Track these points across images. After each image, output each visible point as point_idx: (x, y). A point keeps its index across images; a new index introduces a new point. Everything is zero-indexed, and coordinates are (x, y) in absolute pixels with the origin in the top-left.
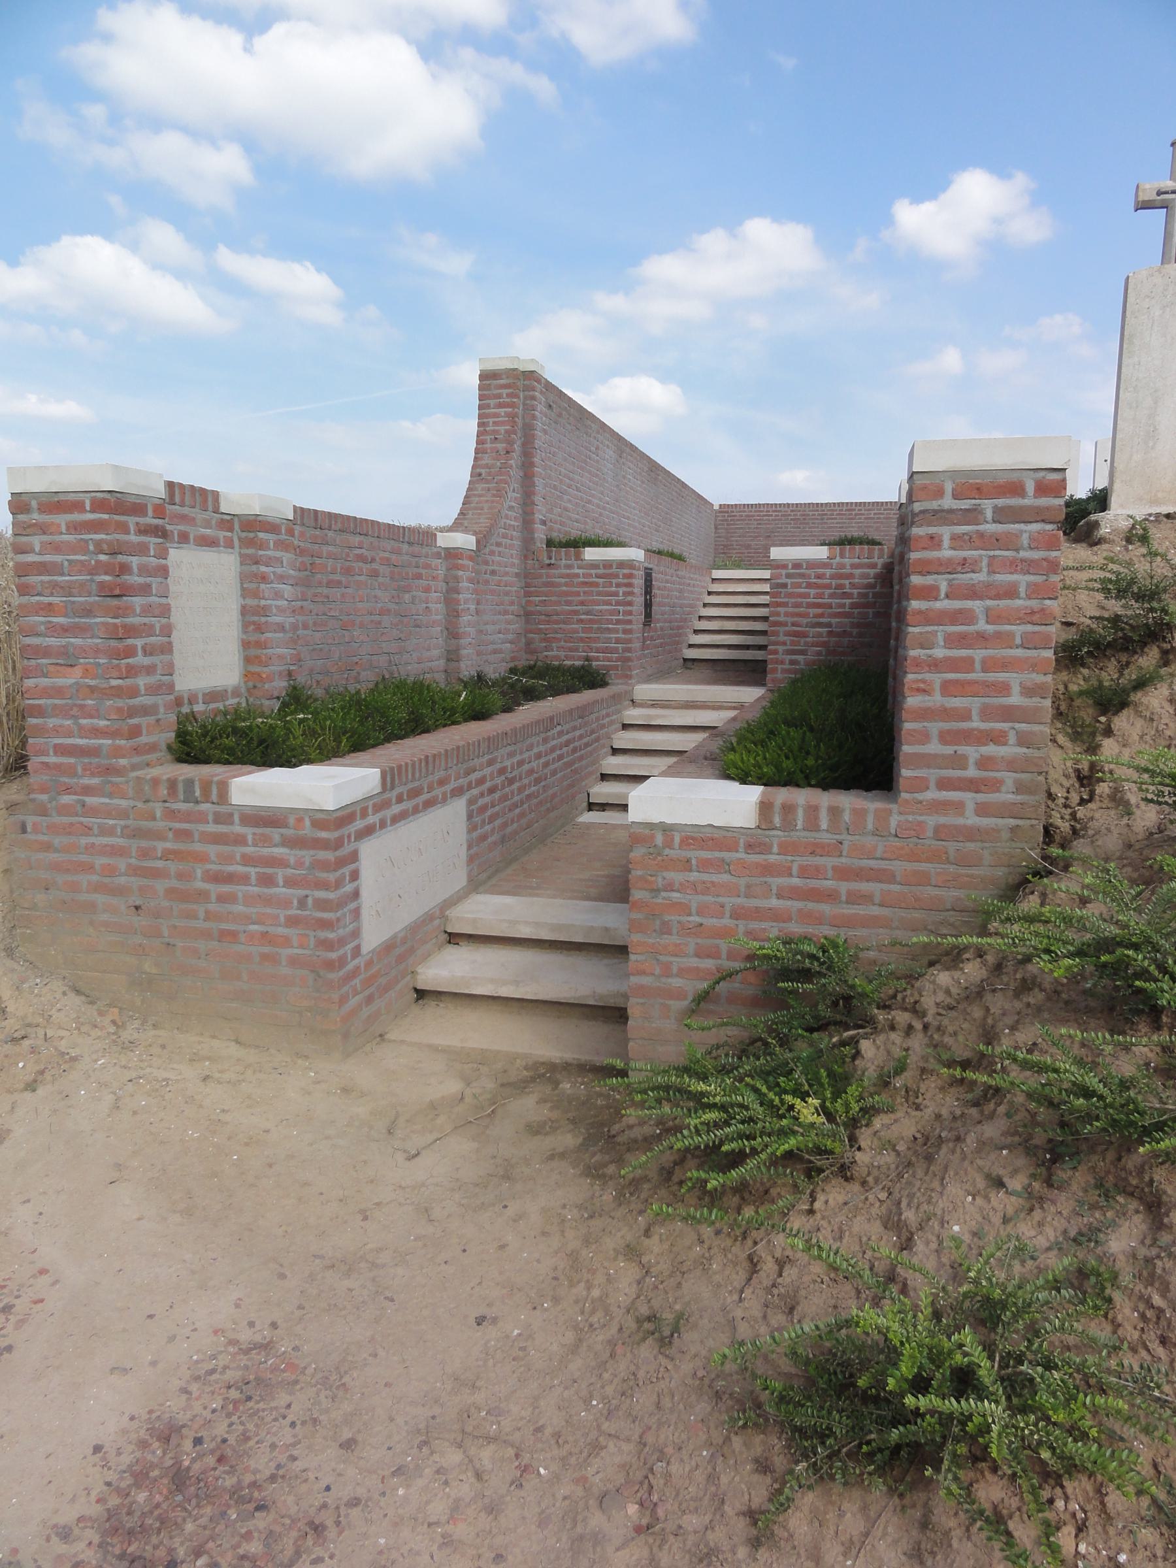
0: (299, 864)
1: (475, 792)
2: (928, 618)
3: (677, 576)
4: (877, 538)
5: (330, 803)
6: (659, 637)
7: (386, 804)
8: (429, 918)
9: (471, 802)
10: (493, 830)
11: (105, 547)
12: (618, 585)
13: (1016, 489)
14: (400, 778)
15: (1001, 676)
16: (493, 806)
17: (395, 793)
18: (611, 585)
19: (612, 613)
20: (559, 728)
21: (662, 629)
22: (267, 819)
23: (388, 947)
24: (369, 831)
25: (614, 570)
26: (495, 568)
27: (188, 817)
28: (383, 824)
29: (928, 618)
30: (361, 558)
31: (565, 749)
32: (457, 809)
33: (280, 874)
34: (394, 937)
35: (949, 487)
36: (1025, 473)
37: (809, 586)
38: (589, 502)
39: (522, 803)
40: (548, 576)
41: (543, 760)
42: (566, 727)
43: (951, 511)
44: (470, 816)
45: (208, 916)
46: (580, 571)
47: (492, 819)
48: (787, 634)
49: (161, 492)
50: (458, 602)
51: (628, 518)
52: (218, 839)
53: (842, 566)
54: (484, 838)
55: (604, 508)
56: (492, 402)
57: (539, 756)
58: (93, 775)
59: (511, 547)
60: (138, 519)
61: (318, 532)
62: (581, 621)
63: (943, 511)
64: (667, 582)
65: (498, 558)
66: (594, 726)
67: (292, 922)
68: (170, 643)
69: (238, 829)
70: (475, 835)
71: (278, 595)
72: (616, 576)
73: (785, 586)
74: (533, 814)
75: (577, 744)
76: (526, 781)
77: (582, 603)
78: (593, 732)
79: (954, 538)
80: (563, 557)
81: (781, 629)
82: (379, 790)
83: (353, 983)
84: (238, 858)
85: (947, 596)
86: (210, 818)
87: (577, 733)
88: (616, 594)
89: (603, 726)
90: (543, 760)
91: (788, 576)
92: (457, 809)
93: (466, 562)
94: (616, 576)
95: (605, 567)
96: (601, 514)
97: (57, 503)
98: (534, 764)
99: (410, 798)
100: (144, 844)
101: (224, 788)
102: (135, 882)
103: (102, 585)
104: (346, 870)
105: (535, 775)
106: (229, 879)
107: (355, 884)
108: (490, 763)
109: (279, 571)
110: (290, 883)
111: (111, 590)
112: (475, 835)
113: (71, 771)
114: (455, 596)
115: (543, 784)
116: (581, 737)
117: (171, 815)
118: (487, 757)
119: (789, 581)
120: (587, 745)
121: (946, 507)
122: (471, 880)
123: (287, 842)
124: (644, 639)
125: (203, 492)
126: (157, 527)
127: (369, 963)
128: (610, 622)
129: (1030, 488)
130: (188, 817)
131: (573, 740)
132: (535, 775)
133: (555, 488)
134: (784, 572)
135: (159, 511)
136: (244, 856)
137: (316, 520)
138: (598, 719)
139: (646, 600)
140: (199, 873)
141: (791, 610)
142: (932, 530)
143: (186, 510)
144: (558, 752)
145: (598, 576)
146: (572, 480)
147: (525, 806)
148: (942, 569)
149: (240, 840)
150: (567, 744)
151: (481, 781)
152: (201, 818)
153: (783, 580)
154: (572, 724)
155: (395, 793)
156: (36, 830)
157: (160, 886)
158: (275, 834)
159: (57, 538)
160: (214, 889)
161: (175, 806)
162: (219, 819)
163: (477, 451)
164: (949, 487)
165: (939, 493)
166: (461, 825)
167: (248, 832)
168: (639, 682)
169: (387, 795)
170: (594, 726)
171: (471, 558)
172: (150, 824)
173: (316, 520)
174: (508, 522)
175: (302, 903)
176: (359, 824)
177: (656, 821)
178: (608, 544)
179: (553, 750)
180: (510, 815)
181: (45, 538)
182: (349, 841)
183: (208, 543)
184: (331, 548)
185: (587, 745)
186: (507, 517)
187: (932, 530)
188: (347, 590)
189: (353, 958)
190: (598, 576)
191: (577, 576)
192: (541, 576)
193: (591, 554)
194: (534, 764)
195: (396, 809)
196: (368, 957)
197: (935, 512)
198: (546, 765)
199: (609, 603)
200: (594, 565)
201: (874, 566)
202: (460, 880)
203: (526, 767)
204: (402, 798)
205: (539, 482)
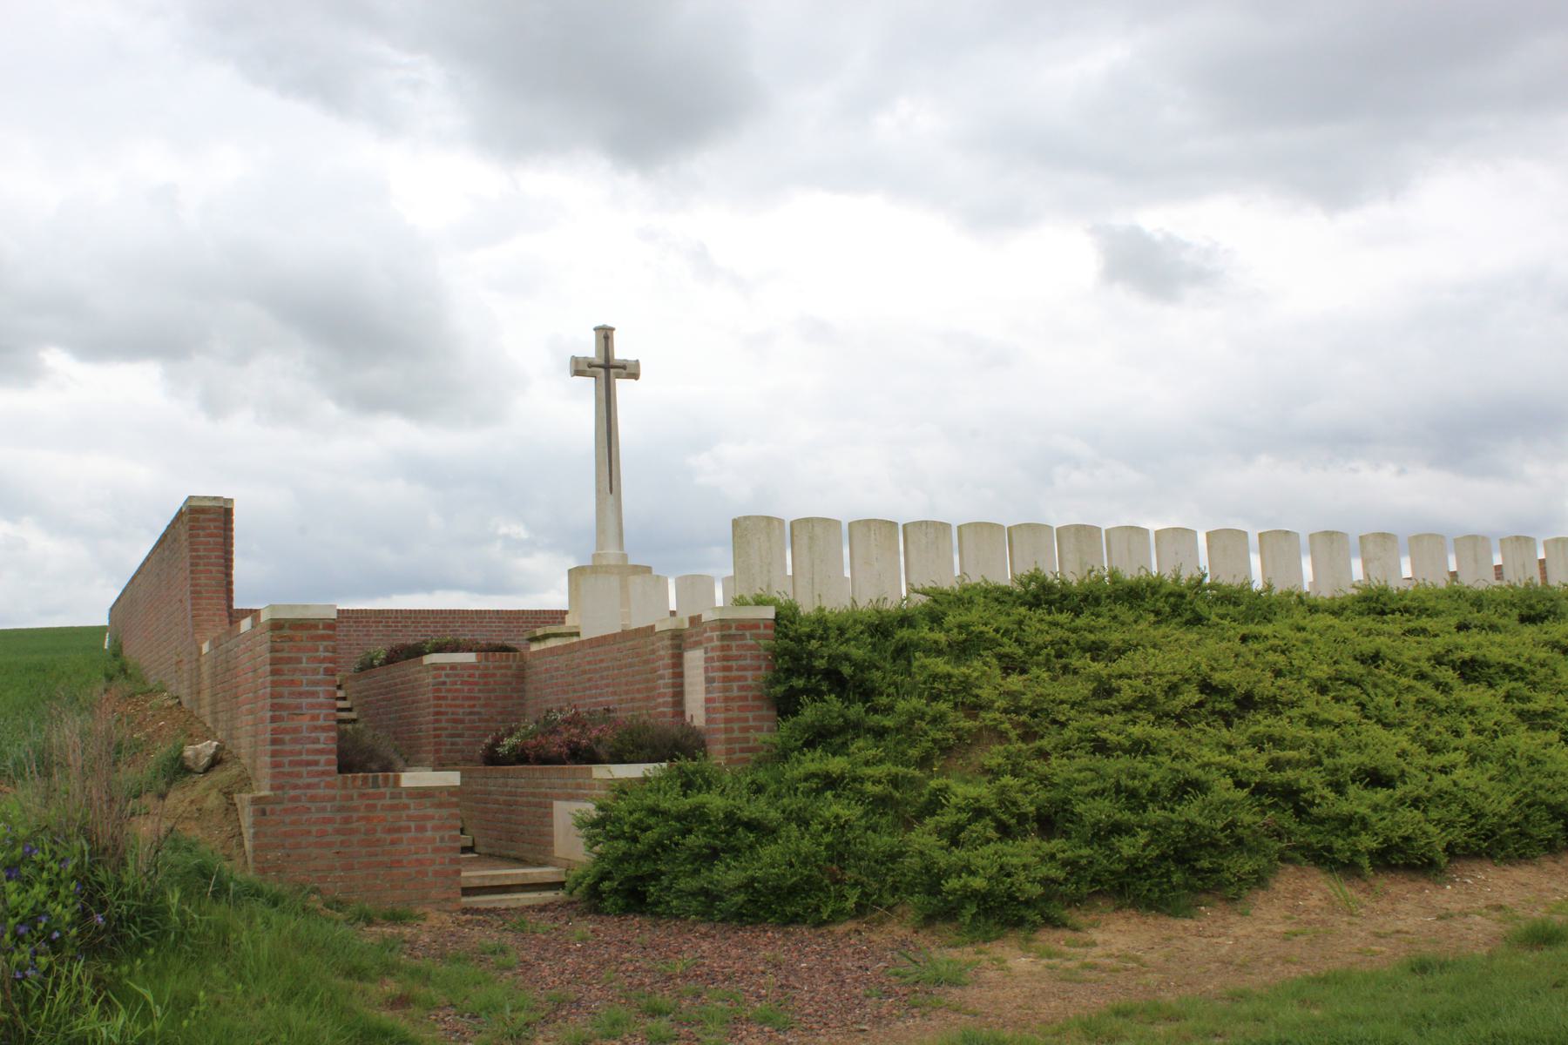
0: (441, 818)
27: (373, 796)
33: (429, 824)
37: (463, 683)
49: (334, 616)
53: (486, 668)
69: (405, 800)
91: (447, 676)
100: (345, 814)
106: (399, 830)
110: (435, 828)
113: (299, 775)
117: (362, 796)
123: (433, 805)
130: (373, 796)
140: (379, 828)
149: (406, 807)
152: (382, 796)
156: (273, 812)
158: (427, 802)
160: (389, 837)
162: (393, 797)
165: (730, 628)
167: (412, 803)
175: (442, 839)
193: (431, 659)
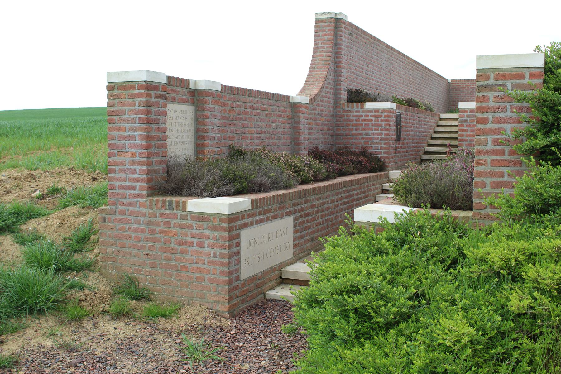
1: (298, 215)
3: (417, 116)
5: (226, 211)
6: (405, 147)
7: (253, 215)
8: (273, 269)
9: (295, 219)
10: (307, 234)
11: (142, 103)
12: (382, 121)
13: (521, 76)
14: (260, 204)
15: (386, 137)
16: (308, 222)
17: (258, 210)
18: (378, 121)
19: (378, 134)
20: (345, 189)
21: (407, 143)
22: (202, 218)
23: (253, 278)
24: (245, 226)
25: (380, 114)
26: (320, 112)
28: (252, 224)
30: (252, 108)
31: (348, 200)
32: (289, 221)
33: (206, 242)
34: (256, 275)
35: (492, 76)
36: (526, 69)
38: (373, 80)
39: (323, 223)
40: (347, 116)
41: (335, 203)
42: (348, 189)
43: (493, 86)
44: (295, 226)
46: (364, 114)
47: (307, 228)
50: (299, 128)
51: (396, 87)
52: (181, 226)
54: (302, 237)
55: (381, 83)
56: (321, 34)
57: (333, 201)
58: (132, 198)
59: (329, 102)
60: (155, 92)
61: (232, 96)
62: (363, 138)
63: (489, 85)
64: (410, 119)
65: (322, 108)
66: (365, 189)
67: (210, 263)
68: (166, 144)
69: (189, 222)
70: (298, 234)
71: (213, 124)
72: (381, 116)
73: (466, 121)
74: (329, 229)
75: (355, 197)
76: (326, 213)
77: (364, 130)
78: (364, 192)
79: (495, 97)
80: (355, 107)
81: (464, 143)
82: (250, 208)
83: (236, 292)
84: (189, 235)
85: (492, 122)
86: (179, 217)
87: (355, 192)
88: (381, 125)
89: (371, 190)
90: (335, 203)
91: (468, 116)
92: (289, 221)
93: (304, 109)
94: (381, 116)
95: (375, 112)
96: (379, 86)
97: (125, 86)
98: (330, 205)
99: (265, 213)
100: (151, 227)
101: (185, 204)
102: (148, 244)
103: (140, 119)
104: (235, 241)
105: (331, 210)
107: (238, 248)
108: (306, 202)
109: (213, 113)
111: (144, 121)
112: (298, 234)
114: (298, 125)
115: (335, 215)
116: (357, 194)
118: (304, 199)
119: (468, 119)
120: (360, 199)
121: (491, 84)
122: (295, 255)
124: (396, 148)
125: (182, 80)
126: (163, 95)
127: (244, 285)
128: (377, 139)
129: (527, 75)
131: (353, 195)
132: (331, 210)
133: (353, 73)
134: (465, 114)
135: (164, 88)
136: (191, 234)
137: (231, 91)
138: (367, 186)
139: (397, 129)
141: (469, 133)
142: (485, 94)
143: (175, 88)
144: (344, 200)
145: (372, 116)
146: (363, 69)
147: (325, 225)
148: (489, 111)
149: (190, 227)
150: (349, 197)
151: (301, 210)
153: (465, 118)
154: (352, 187)
155: (258, 210)
157: (158, 245)
159: (124, 101)
160: (179, 248)
161: (164, 212)
163: (313, 56)
164: (492, 76)
166: (291, 229)
168: (392, 170)
169: (254, 211)
170: (365, 189)
171: (306, 108)
172: (154, 220)
173: (231, 91)
174: (327, 90)
175: (215, 255)
176: (241, 222)
177: (366, 221)
179: (341, 199)
180: (317, 228)
181: (119, 100)
182: (236, 229)
183: (184, 102)
184: (237, 103)
185: (360, 199)
186: (327, 88)
187: (485, 94)
188: (245, 122)
189: (236, 281)
190: (372, 116)
191: (362, 116)
192: (344, 116)
193: (368, 105)
194: (330, 205)
195: (258, 218)
196: (243, 282)
197: (486, 86)
198: (337, 206)
199: (377, 130)
200: (370, 111)
202: (289, 254)
203: (326, 206)
204: (262, 213)
205: (344, 72)
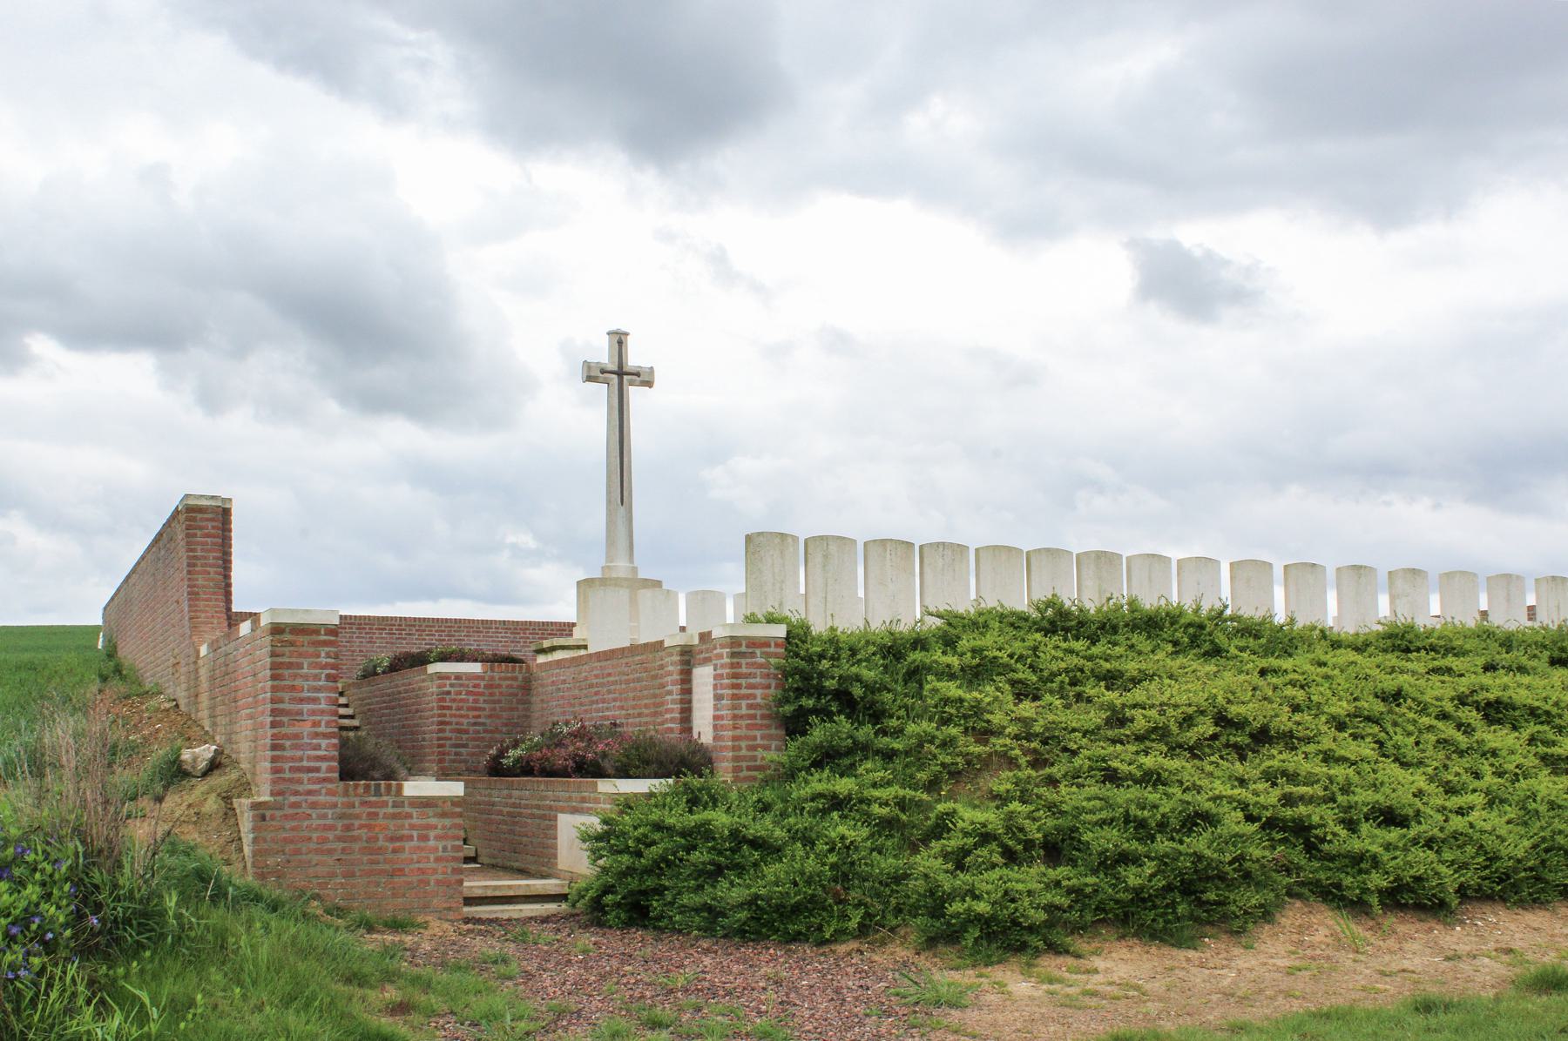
2: (331, 759)
4: (517, 655)
29: (331, 759)
33: (432, 834)
45: (386, 861)
48: (452, 731)
69: (407, 809)
91: (452, 685)
100: (346, 822)
106: (401, 839)
117: (364, 804)
140: (381, 837)
149: (409, 816)
152: (385, 804)
158: (430, 811)
160: (390, 846)
167: (414, 812)
172: (351, 811)
175: (445, 849)
178: (977, 576)
193: (434, 668)
201: (515, 679)
